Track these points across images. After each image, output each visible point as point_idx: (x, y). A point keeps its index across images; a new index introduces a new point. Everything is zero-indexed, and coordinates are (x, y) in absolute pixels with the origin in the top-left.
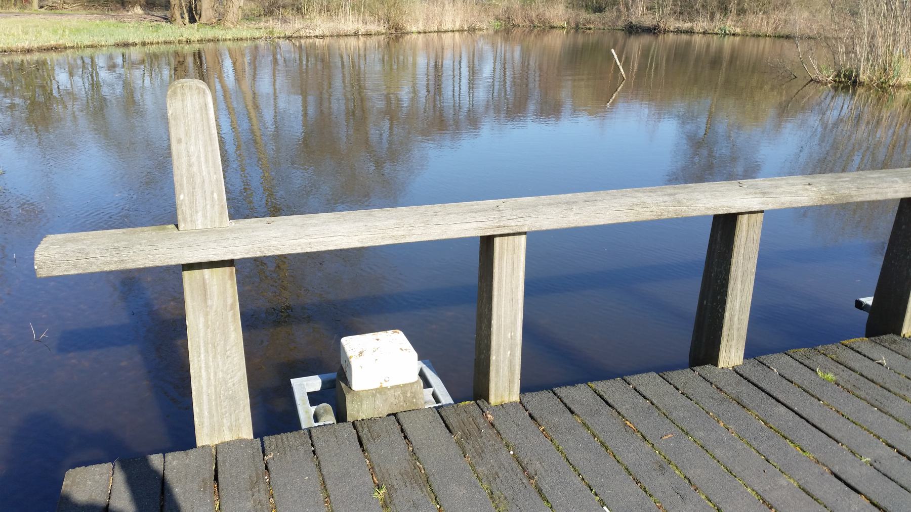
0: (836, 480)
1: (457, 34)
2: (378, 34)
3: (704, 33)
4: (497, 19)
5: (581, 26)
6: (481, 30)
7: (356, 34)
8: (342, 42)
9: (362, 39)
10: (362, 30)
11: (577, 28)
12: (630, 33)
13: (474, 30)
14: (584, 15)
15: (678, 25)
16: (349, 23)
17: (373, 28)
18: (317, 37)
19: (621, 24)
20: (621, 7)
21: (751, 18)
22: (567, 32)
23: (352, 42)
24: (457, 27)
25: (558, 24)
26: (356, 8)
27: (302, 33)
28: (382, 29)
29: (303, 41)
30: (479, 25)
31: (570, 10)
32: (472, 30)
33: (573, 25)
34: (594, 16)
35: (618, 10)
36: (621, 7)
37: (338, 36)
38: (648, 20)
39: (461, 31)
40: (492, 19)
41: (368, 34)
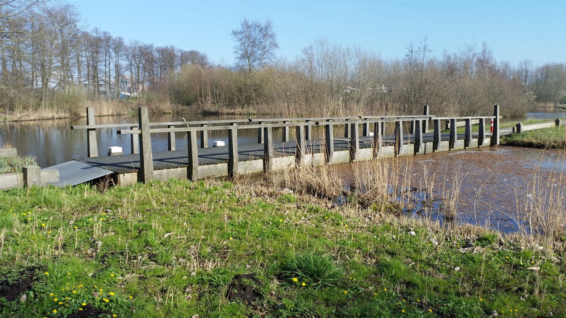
0: (87, 170)
1: (110, 118)
2: (65, 118)
3: (240, 114)
4: (133, 109)
5: (179, 112)
6: (124, 115)
7: (53, 119)
8: (44, 122)
9: (56, 121)
10: (56, 116)
11: (178, 113)
12: (205, 115)
13: (120, 115)
14: (180, 107)
15: (227, 111)
16: (47, 113)
17: (62, 115)
18: (31, 120)
19: (200, 111)
20: (200, 103)
21: (261, 106)
22: (173, 116)
23: (50, 122)
24: (110, 113)
25: (167, 112)
26: (51, 106)
27: (23, 119)
28: (67, 115)
29: (23, 123)
30: (123, 112)
31: (173, 105)
32: (119, 115)
33: (175, 112)
34: (185, 107)
35: (198, 104)
36: (200, 103)
37: (43, 119)
38: (213, 109)
39: (113, 115)
40: (130, 110)
41: (60, 118)
